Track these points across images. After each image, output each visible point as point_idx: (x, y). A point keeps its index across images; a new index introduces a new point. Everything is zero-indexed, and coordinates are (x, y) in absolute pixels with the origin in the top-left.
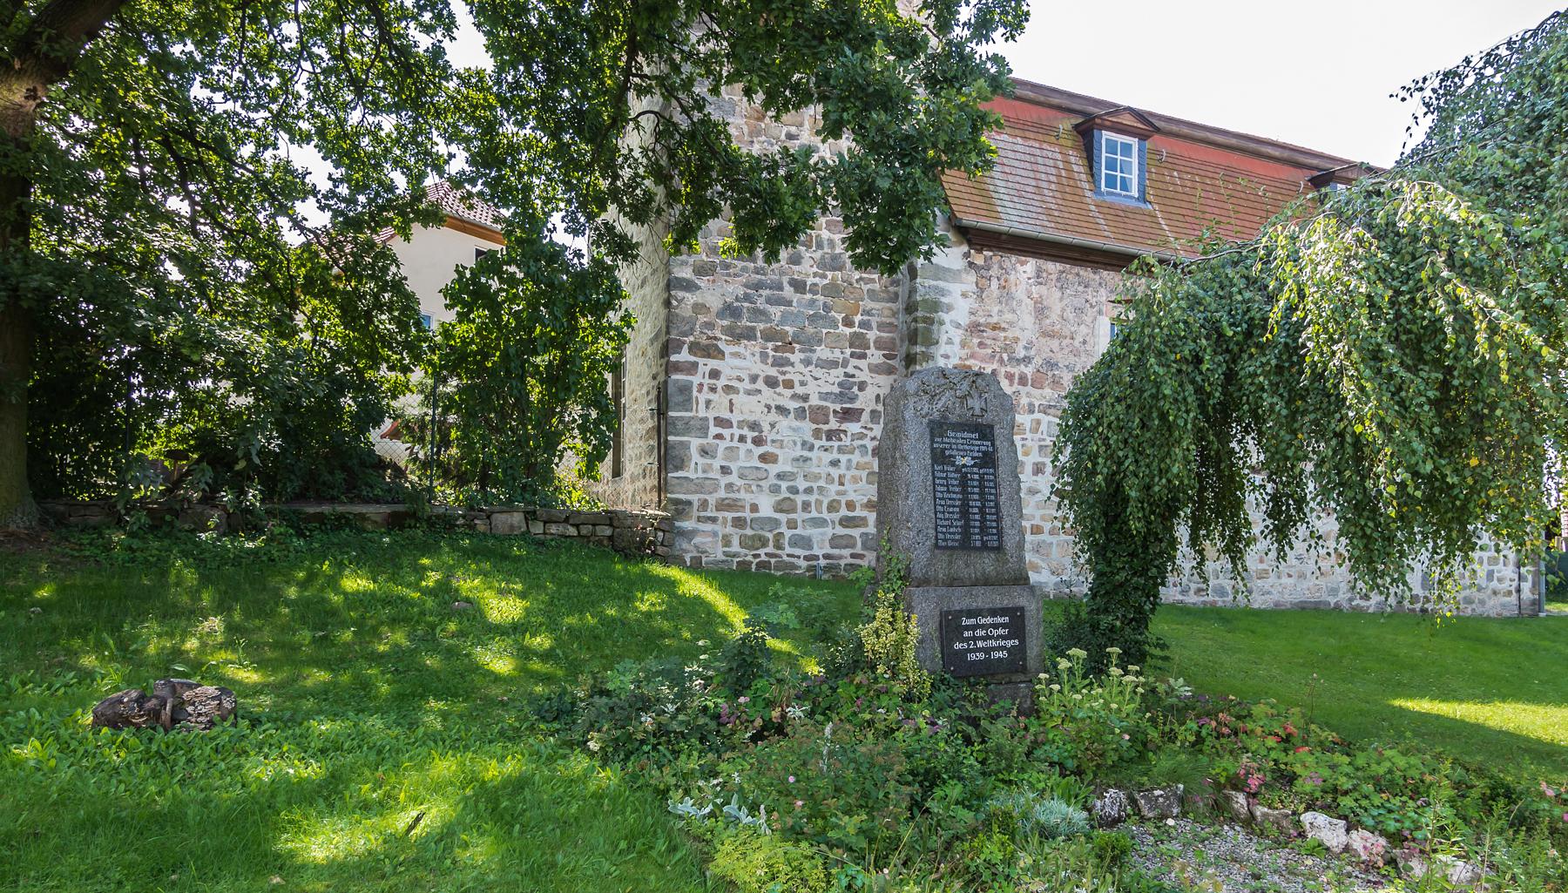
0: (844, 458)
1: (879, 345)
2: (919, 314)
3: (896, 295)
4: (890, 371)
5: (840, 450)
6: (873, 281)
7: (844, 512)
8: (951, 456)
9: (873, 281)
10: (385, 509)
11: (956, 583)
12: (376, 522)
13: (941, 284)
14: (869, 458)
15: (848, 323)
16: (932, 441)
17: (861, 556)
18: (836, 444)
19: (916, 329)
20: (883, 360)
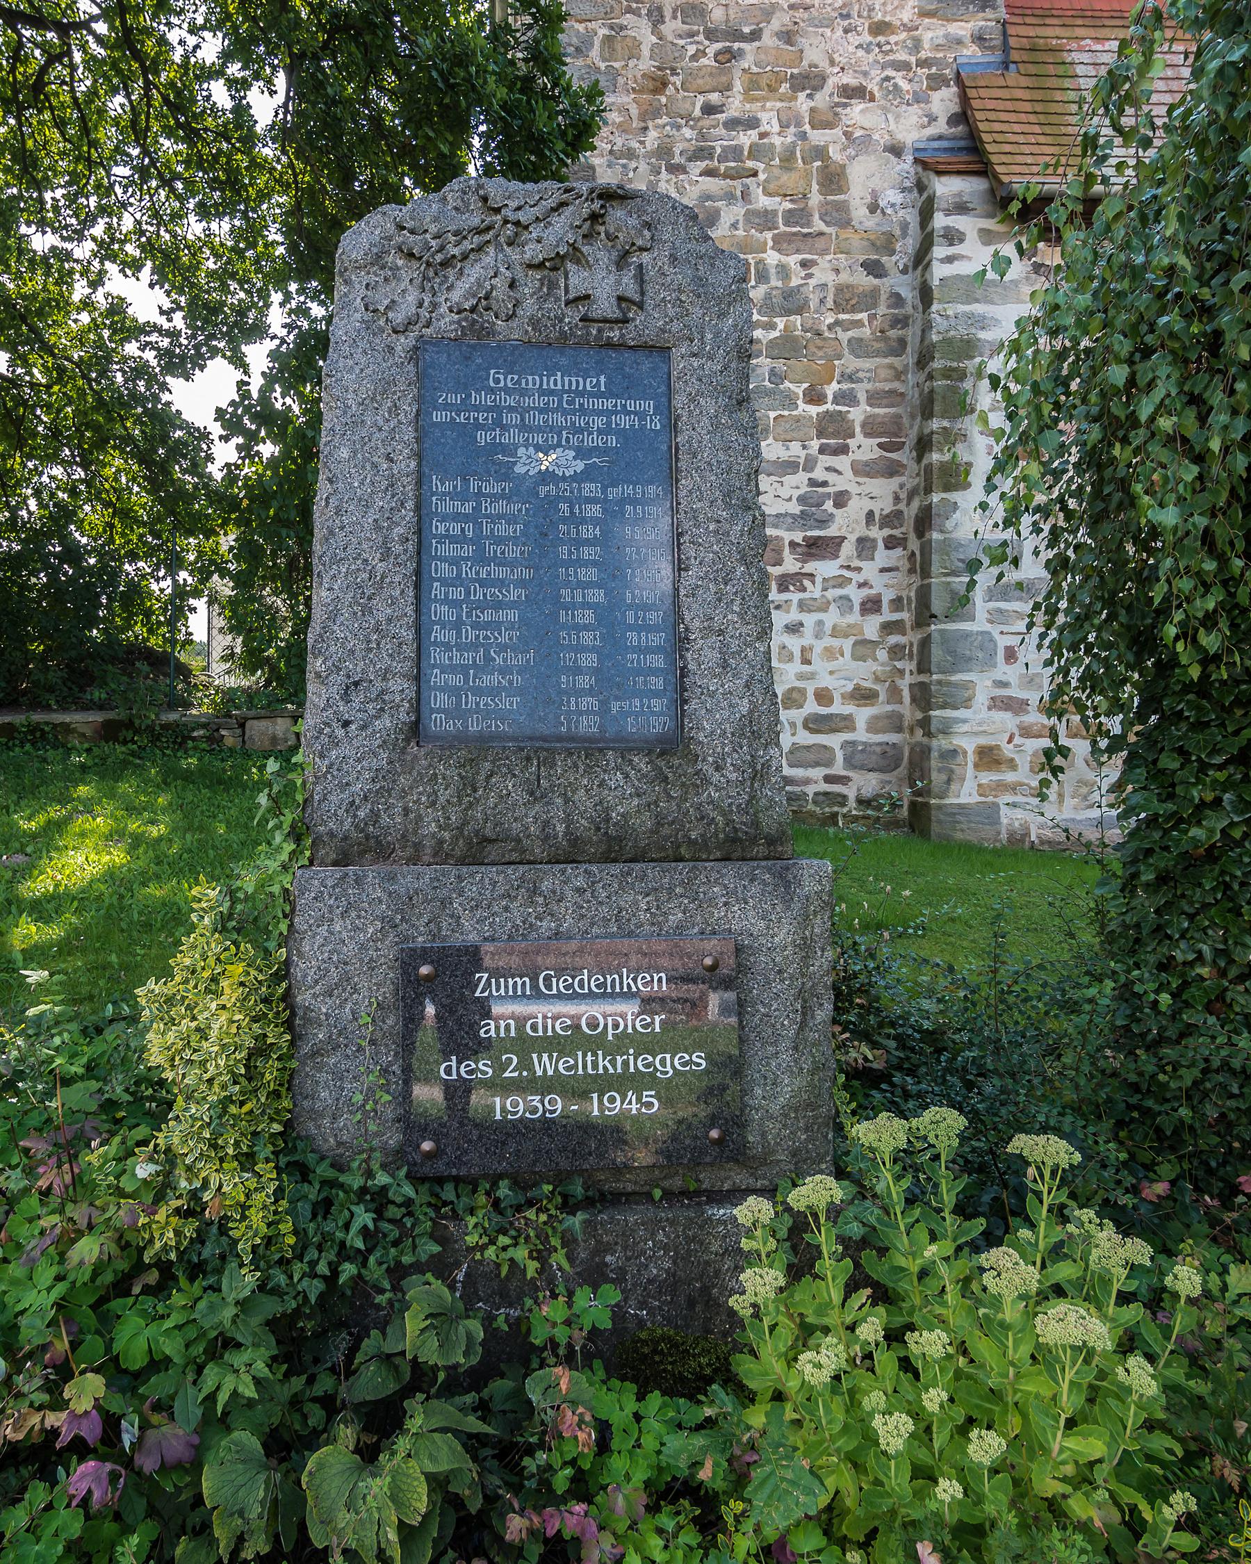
0: (809, 620)
1: (870, 428)
2: (937, 364)
3: (902, 342)
4: (892, 470)
5: (803, 606)
6: (859, 324)
7: (811, 707)
8: (495, 447)
9: (859, 324)
10: (97, 717)
11: (493, 852)
12: (83, 735)
13: (978, 308)
14: (854, 617)
15: (814, 397)
16: (423, 404)
17: (843, 780)
18: (795, 597)
19: (932, 391)
20: (878, 453)
